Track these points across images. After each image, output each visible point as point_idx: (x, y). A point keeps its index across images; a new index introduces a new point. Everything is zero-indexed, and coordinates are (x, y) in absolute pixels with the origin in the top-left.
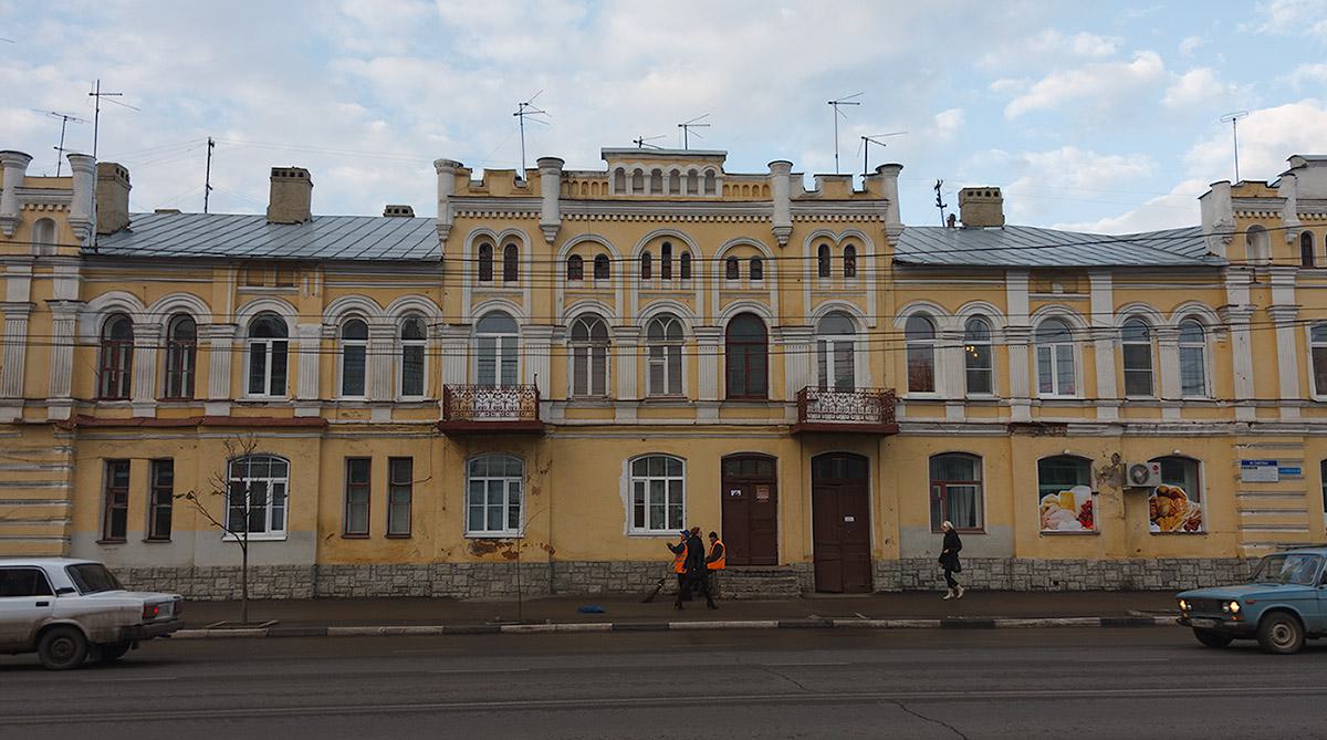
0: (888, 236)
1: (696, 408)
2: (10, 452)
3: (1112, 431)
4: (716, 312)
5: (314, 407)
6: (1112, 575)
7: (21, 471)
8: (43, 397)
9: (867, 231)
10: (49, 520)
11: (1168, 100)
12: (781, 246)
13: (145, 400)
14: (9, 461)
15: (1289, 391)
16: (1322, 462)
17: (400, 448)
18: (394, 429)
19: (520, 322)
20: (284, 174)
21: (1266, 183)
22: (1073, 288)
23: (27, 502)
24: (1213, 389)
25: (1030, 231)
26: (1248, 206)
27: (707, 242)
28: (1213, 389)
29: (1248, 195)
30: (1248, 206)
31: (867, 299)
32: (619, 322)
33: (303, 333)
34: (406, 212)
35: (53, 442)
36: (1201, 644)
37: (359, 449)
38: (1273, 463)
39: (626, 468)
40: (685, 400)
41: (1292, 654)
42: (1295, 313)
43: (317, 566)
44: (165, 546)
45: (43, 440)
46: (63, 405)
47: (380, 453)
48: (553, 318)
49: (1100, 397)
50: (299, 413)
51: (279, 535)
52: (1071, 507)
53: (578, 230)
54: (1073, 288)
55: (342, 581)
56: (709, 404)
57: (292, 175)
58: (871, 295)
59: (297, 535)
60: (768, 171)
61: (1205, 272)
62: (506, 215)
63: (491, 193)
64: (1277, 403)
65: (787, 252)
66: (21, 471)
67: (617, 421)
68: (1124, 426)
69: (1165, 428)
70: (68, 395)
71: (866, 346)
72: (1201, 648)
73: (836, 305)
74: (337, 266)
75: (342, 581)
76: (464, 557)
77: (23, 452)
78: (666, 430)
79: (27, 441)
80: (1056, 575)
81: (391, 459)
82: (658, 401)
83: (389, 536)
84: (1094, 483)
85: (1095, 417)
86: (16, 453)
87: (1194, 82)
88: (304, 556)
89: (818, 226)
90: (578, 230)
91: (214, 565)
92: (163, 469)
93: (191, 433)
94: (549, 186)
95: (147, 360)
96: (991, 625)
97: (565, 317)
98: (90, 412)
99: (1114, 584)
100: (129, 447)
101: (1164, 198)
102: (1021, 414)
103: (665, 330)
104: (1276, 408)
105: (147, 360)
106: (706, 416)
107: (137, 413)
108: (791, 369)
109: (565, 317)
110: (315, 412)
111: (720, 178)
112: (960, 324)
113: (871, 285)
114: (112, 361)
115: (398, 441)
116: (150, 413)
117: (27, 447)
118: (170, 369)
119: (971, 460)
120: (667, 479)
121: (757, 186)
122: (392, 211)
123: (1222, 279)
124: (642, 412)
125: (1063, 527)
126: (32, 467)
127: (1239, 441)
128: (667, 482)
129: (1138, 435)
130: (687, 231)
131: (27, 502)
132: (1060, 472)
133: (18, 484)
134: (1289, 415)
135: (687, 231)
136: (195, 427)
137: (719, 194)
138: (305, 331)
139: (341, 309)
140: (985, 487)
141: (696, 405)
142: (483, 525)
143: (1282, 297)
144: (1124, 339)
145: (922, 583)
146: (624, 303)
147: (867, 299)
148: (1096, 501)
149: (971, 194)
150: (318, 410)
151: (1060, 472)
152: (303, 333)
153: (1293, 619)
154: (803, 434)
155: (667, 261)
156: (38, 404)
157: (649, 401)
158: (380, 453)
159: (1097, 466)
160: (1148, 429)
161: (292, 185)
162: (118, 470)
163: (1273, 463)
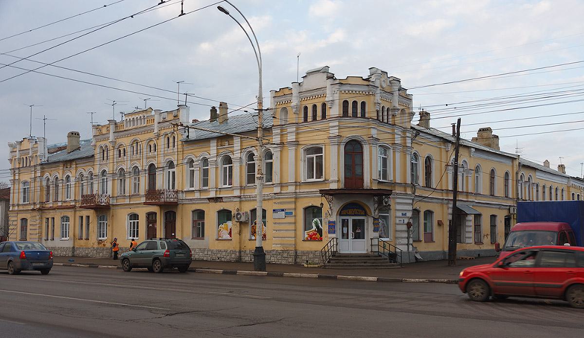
3: (235, 200)
6: (233, 256)
21: (362, 77)
26: (313, 94)
29: (281, 94)
30: (313, 94)
38: (283, 210)
39: (127, 218)
43: (74, 247)
44: (432, 243)
48: (113, 171)
52: (227, 230)
63: (103, 133)
69: (253, 197)
76: (96, 246)
80: (219, 255)
85: (195, 196)
88: (70, 244)
94: (112, 128)
96: (282, 276)
97: (116, 170)
98: (44, 206)
99: (234, 259)
109: (116, 170)
123: (233, 138)
125: (224, 237)
129: (246, 201)
132: (225, 215)
149: (73, 134)
150: (279, 188)
151: (225, 215)
153: (476, 280)
157: (133, 195)
160: (248, 198)
163: (283, 210)
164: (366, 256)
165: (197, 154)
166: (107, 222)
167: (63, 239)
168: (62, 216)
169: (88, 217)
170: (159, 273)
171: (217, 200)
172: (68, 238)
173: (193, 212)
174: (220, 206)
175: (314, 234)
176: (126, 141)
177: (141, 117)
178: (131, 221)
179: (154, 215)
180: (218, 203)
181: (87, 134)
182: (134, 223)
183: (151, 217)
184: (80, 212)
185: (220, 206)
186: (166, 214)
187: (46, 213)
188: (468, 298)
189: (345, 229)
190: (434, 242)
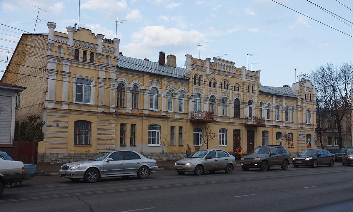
0: (259, 85)
1: (98, 107)
2: (101, 120)
4: (233, 98)
5: (165, 113)
7: (104, 126)
8: (61, 101)
9: (256, 83)
10: (112, 140)
11: (127, 17)
12: (99, 59)
13: (129, 108)
14: (101, 123)
15: (65, 99)
16: (234, 130)
17: (181, 124)
18: (181, 120)
19: (202, 96)
20: (109, 41)
22: (152, 79)
23: (106, 134)
24: (295, 121)
25: (127, 58)
26: (238, 76)
27: (233, 82)
28: (295, 121)
31: (256, 100)
32: (218, 98)
33: (163, 94)
34: (287, 86)
35: (111, 118)
36: (178, 174)
37: (173, 124)
40: (227, 117)
41: (95, 182)
42: (70, 75)
44: (135, 147)
45: (109, 117)
46: (113, 108)
47: (177, 125)
49: (63, 101)
50: (163, 114)
51: (158, 145)
52: (279, 142)
53: (212, 76)
54: (152, 79)
55: (171, 156)
56: (232, 118)
57: (109, 41)
58: (256, 97)
59: (163, 145)
60: (241, 68)
61: (292, 98)
62: (200, 70)
64: (60, 103)
65: (100, 61)
66: (104, 126)
67: (99, 111)
68: (286, 127)
70: (114, 105)
71: (255, 107)
72: (178, 175)
73: (252, 99)
74: (131, 72)
75: (171, 156)
77: (104, 121)
78: (63, 111)
79: (106, 117)
81: (179, 127)
82: (223, 117)
83: (179, 146)
84: (282, 137)
86: (103, 120)
87: (134, 14)
89: (249, 82)
90: (212, 76)
91: (148, 152)
92: (133, 126)
93: (141, 118)
95: (129, 96)
100: (126, 121)
101: (124, 47)
102: (274, 124)
103: (224, 100)
104: (302, 125)
105: (129, 96)
106: (231, 121)
107: (127, 111)
108: (244, 112)
110: (165, 114)
111: (234, 68)
112: (131, 86)
113: (256, 95)
114: (135, 99)
115: (181, 123)
116: (130, 112)
117: (105, 119)
118: (137, 102)
119: (88, 123)
120: (152, 131)
121: (239, 70)
122: (146, 59)
124: (56, 104)
126: (107, 125)
127: (299, 130)
128: (152, 132)
130: (229, 79)
131: (106, 134)
132: (279, 135)
133: (104, 129)
134: (65, 107)
135: (229, 79)
136: (142, 116)
137: (234, 72)
138: (163, 92)
139: (170, 88)
140: (269, 139)
141: (230, 118)
142: (155, 143)
143: (66, 69)
144: (76, 83)
145: (52, 161)
146: (219, 94)
147: (256, 100)
148: (282, 141)
152: (163, 94)
153: (98, 173)
154: (246, 126)
155: (225, 85)
156: (107, 107)
158: (177, 125)
159: (283, 134)
161: (172, 59)
162: (172, 128)
163: (302, 135)
164: (37, 152)
165: (266, 101)
166: (201, 133)
167: (150, 145)
168: (151, 123)
169: (180, 128)
170: (267, 170)
171: (276, 127)
172: (156, 145)
173: (75, 121)
174: (278, 130)
175: (309, 145)
176: (219, 79)
177: (230, 66)
178: (220, 134)
179: (238, 132)
180: (277, 129)
181: (181, 62)
182: (223, 135)
183: (237, 133)
184: (172, 123)
185: (278, 130)
186: (248, 132)
187: (122, 118)
188: (225, 172)
189: (226, 143)
190: (136, 146)
